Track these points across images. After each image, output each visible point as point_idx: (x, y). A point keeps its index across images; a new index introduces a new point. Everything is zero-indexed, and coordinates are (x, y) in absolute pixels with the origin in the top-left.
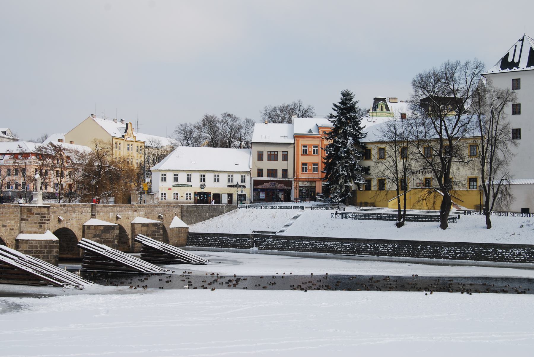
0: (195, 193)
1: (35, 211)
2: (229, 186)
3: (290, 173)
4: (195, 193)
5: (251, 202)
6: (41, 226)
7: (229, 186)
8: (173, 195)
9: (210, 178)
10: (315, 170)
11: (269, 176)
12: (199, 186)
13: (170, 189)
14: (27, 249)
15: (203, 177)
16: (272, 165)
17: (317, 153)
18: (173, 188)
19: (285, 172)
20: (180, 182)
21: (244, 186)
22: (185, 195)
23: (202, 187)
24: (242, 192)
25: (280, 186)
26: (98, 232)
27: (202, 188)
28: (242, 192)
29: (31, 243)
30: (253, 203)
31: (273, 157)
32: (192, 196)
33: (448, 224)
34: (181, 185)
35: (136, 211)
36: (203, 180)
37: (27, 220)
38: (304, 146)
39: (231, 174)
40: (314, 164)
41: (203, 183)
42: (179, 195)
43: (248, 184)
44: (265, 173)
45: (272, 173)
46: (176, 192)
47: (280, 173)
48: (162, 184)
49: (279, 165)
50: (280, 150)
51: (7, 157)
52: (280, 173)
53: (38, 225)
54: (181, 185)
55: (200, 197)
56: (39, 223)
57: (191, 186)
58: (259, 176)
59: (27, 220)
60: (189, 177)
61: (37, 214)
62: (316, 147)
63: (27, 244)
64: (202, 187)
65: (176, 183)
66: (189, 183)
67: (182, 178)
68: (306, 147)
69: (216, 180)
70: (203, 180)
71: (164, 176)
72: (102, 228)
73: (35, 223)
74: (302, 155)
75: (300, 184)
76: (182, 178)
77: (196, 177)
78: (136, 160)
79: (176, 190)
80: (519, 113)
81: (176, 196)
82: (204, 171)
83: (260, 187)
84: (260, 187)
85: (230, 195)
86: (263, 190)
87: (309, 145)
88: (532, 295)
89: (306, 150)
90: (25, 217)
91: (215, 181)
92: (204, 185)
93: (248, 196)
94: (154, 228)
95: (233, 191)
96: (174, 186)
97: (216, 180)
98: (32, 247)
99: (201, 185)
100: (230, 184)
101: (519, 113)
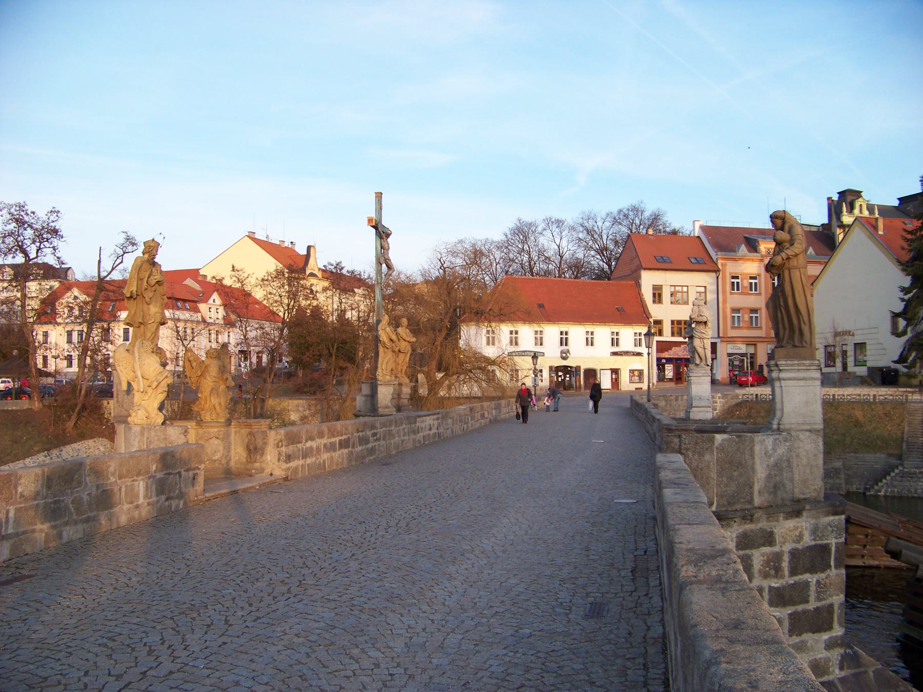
0: (551, 368)
2: (615, 354)
4: (551, 368)
10: (753, 324)
11: (673, 334)
15: (539, 336)
17: (756, 290)
20: (622, 347)
23: (564, 355)
27: (564, 358)
38: (733, 277)
41: (564, 347)
44: (667, 328)
51: (660, 630)
55: (558, 376)
62: (755, 278)
64: (564, 355)
68: (737, 278)
71: (514, 335)
74: (731, 293)
75: (731, 348)
78: (111, 338)
79: (617, 362)
83: (666, 355)
84: (666, 355)
85: (615, 371)
86: (669, 361)
89: (738, 283)
91: (587, 344)
92: (568, 351)
95: (617, 362)
99: (562, 352)
100: (616, 349)
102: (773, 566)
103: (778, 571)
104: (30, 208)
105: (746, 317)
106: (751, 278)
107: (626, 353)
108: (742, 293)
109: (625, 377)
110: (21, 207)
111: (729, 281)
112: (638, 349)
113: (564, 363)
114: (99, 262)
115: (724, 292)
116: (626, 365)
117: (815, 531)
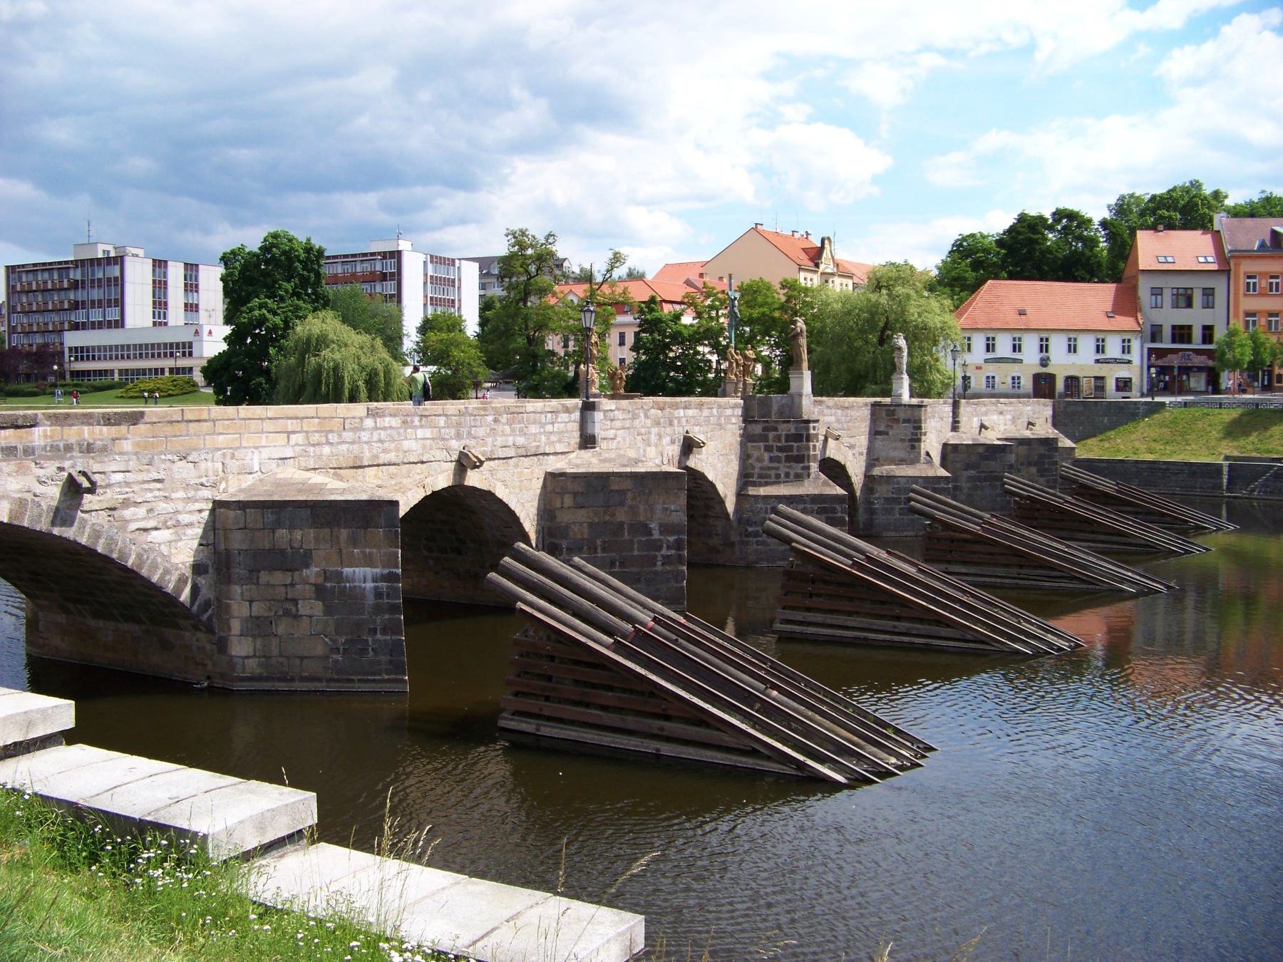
1: (901, 414)
2: (1097, 361)
3: (1219, 335)
5: (1142, 395)
6: (913, 447)
7: (1097, 361)
8: (984, 380)
9: (1058, 346)
11: (1174, 341)
12: (1038, 362)
13: (979, 368)
14: (890, 495)
16: (1182, 317)
18: (986, 366)
19: (1208, 332)
21: (1129, 362)
22: (1009, 381)
23: (1044, 362)
25: (1198, 360)
26: (973, 458)
29: (898, 483)
30: (1147, 396)
31: (1185, 299)
34: (1107, 361)
35: (1001, 413)
36: (1044, 348)
37: (887, 434)
38: (1249, 277)
39: (1072, 336)
40: (1271, 315)
41: (1044, 354)
42: (997, 379)
43: (1135, 356)
44: (1167, 332)
45: (1182, 333)
46: (991, 374)
47: (1197, 334)
49: (1195, 317)
50: (1197, 284)
52: (1197, 334)
53: (907, 444)
54: (1107, 361)
56: (910, 440)
57: (1020, 361)
58: (1204, 342)
59: (887, 434)
61: (905, 421)
63: (889, 483)
64: (1044, 362)
65: (990, 355)
67: (1004, 347)
68: (1254, 277)
69: (1072, 349)
70: (1044, 348)
72: (981, 450)
73: (902, 440)
76: (1004, 347)
77: (1030, 346)
79: (991, 370)
87: (1260, 274)
88: (364, 497)
90: (882, 428)
92: (1048, 358)
93: (1136, 381)
94: (1042, 450)
95: (1102, 370)
96: (986, 361)
97: (1072, 349)
98: (899, 490)
99: (1042, 360)
100: (1100, 356)
102: (778, 438)
103: (780, 440)
104: (530, 233)
105: (1263, 321)
106: (1272, 277)
107: (1116, 361)
108: (1261, 295)
109: (1111, 385)
110: (523, 233)
111: (1242, 281)
112: (1127, 357)
113: (1044, 370)
114: (487, 934)
115: (1236, 294)
116: (1113, 374)
117: (796, 429)
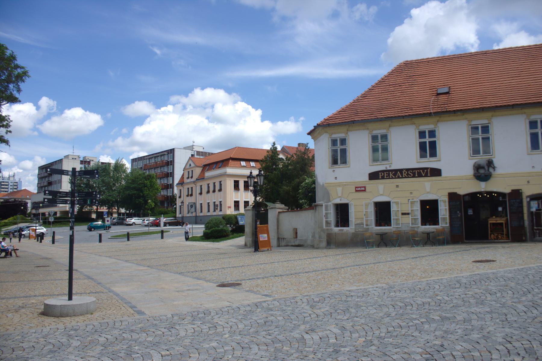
12: (470, 171)
13: (361, 189)
24: (230, 207)
28: (230, 207)
32: (444, 211)
33: (71, 170)
48: (343, 174)
54: (398, 174)
57: (436, 172)
60: (427, 140)
64: (483, 172)
66: (429, 163)
71: (339, 147)
79: (382, 192)
80: (424, 203)
81: (383, 212)
82: (483, 110)
92: (490, 163)
96: (374, 176)
99: (477, 168)
101: (424, 203)
